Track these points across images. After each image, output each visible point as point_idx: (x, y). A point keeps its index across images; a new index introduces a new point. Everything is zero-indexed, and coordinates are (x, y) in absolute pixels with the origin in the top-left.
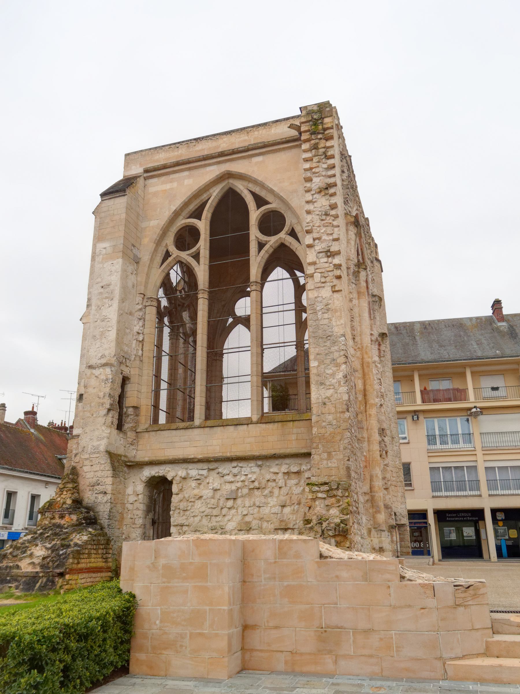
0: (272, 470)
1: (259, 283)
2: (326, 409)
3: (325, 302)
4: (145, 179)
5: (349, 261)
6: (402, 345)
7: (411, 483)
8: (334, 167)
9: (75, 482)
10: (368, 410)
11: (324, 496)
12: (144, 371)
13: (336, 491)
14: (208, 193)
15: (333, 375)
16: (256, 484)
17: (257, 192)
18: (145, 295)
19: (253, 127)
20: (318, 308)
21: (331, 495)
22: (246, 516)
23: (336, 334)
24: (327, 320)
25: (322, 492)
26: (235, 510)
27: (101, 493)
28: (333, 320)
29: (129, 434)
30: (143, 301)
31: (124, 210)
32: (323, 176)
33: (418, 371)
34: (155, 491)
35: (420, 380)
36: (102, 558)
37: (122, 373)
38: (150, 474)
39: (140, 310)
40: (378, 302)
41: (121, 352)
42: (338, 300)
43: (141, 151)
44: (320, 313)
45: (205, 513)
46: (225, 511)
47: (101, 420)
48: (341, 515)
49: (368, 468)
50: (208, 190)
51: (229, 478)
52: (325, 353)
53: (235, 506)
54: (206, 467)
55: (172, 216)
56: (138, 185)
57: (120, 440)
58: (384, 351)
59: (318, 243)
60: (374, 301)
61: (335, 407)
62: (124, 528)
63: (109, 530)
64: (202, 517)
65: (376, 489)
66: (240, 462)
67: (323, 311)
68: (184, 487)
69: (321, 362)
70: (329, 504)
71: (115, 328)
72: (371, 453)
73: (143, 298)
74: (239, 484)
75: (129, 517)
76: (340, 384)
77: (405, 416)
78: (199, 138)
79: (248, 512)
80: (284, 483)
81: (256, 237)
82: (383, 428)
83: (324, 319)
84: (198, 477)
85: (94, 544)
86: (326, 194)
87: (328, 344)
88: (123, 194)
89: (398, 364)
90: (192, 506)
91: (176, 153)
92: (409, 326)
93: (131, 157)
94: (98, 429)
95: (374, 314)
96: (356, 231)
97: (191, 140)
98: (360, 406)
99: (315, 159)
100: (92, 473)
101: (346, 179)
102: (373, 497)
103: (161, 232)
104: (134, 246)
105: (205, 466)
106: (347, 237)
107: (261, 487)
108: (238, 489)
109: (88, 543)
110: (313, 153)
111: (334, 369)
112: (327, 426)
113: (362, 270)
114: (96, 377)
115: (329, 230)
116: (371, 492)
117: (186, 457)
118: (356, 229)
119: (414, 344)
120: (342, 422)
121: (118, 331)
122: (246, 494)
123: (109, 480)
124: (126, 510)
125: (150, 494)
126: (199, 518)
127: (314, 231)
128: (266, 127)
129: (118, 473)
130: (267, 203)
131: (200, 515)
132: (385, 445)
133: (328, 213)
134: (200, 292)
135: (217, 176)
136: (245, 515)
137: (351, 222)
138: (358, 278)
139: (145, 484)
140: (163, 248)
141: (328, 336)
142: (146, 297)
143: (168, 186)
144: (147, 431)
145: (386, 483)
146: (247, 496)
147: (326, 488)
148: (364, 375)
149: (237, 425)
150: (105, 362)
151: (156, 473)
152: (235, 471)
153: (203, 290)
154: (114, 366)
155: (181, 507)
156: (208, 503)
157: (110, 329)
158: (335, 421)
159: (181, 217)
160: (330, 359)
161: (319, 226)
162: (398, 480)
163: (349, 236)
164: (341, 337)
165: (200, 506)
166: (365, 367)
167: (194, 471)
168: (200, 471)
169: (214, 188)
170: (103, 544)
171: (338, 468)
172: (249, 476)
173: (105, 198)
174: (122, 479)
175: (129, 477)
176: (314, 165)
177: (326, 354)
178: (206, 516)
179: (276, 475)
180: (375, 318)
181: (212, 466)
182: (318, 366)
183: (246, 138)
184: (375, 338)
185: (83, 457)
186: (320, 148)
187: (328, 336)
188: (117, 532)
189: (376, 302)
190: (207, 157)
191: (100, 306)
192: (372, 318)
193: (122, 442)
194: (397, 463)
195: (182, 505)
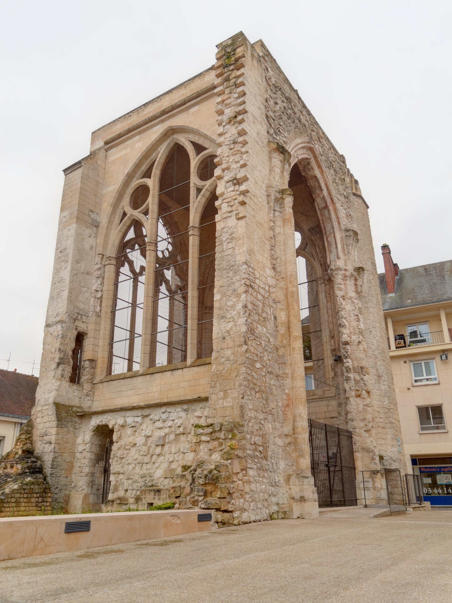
0: (196, 414)
1: (196, 227)
2: (225, 344)
3: (230, 231)
4: (107, 150)
5: (269, 188)
6: (430, 285)
7: (445, 426)
8: (245, 94)
9: (28, 433)
10: (291, 343)
11: (208, 439)
12: (101, 326)
13: (219, 433)
15: (233, 306)
16: (181, 429)
17: (196, 142)
18: (104, 255)
19: (190, 80)
20: (224, 239)
21: (214, 438)
22: (173, 463)
23: (238, 262)
24: (231, 250)
25: (206, 435)
26: (163, 457)
28: (236, 249)
30: (102, 261)
32: (234, 106)
33: (444, 309)
34: (108, 440)
35: (447, 318)
36: (36, 506)
37: (76, 329)
38: (96, 423)
39: (99, 269)
40: (352, 237)
41: (75, 309)
42: (241, 227)
43: (104, 127)
44: (226, 243)
45: (137, 461)
46: (155, 457)
47: (52, 374)
48: (222, 460)
49: (292, 407)
50: (156, 149)
51: (159, 424)
52: (227, 285)
53: (163, 453)
54: (140, 414)
56: (97, 156)
58: (361, 286)
59: (227, 173)
60: (347, 236)
61: (233, 341)
62: (74, 476)
63: (51, 479)
64: (135, 465)
65: (299, 430)
66: (168, 407)
67: (228, 241)
68: (122, 434)
69: (224, 295)
70: (212, 448)
72: (294, 390)
73: (102, 258)
74: (167, 430)
75: (78, 466)
76: (239, 315)
77: (432, 356)
79: (174, 458)
82: (361, 366)
83: (229, 249)
84: (133, 425)
85: (25, 493)
86: (235, 123)
87: (231, 274)
88: (79, 166)
89: (422, 304)
90: (127, 454)
91: (129, 121)
92: (439, 266)
93: (96, 134)
94: (49, 382)
95: (348, 248)
96: (281, 158)
97: (141, 106)
98: (282, 339)
99: (227, 91)
100: (42, 424)
101: (279, 110)
102: (296, 439)
103: (117, 195)
104: (92, 212)
105: (139, 413)
107: (186, 432)
108: (166, 436)
109: (16, 491)
110: (225, 86)
112: (225, 362)
113: (287, 196)
114: (51, 334)
115: (237, 158)
116: (294, 434)
117: (123, 406)
118: (282, 155)
119: (442, 283)
120: (239, 356)
122: (173, 440)
123: (54, 431)
124: (76, 459)
125: (100, 443)
126: (133, 465)
127: (224, 162)
129: (65, 423)
130: (205, 149)
131: (133, 462)
132: (364, 384)
133: (236, 141)
134: (147, 244)
137: (274, 149)
138: (282, 206)
139: (93, 434)
142: (105, 257)
143: (123, 153)
144: (101, 382)
145: (366, 425)
146: (174, 442)
147: (210, 430)
148: (288, 305)
149: (173, 370)
150: (59, 319)
151: (100, 422)
152: (164, 416)
153: (150, 242)
154: (65, 322)
155: (118, 455)
156: (140, 451)
157: (64, 289)
158: (233, 356)
159: (135, 179)
160: (231, 291)
161: (228, 156)
162: (387, 421)
163: (273, 164)
164: (243, 265)
166: (289, 297)
168: (136, 418)
169: (162, 146)
170: (38, 493)
171: (232, 407)
172: (176, 421)
174: (72, 429)
175: (81, 427)
176: (226, 96)
178: (139, 463)
179: (200, 418)
180: (349, 253)
182: (221, 299)
183: (184, 92)
184: (350, 273)
185: (37, 410)
186: (232, 79)
188: (63, 481)
189: (350, 236)
190: (152, 118)
192: (346, 253)
194: (385, 403)
195: (120, 453)
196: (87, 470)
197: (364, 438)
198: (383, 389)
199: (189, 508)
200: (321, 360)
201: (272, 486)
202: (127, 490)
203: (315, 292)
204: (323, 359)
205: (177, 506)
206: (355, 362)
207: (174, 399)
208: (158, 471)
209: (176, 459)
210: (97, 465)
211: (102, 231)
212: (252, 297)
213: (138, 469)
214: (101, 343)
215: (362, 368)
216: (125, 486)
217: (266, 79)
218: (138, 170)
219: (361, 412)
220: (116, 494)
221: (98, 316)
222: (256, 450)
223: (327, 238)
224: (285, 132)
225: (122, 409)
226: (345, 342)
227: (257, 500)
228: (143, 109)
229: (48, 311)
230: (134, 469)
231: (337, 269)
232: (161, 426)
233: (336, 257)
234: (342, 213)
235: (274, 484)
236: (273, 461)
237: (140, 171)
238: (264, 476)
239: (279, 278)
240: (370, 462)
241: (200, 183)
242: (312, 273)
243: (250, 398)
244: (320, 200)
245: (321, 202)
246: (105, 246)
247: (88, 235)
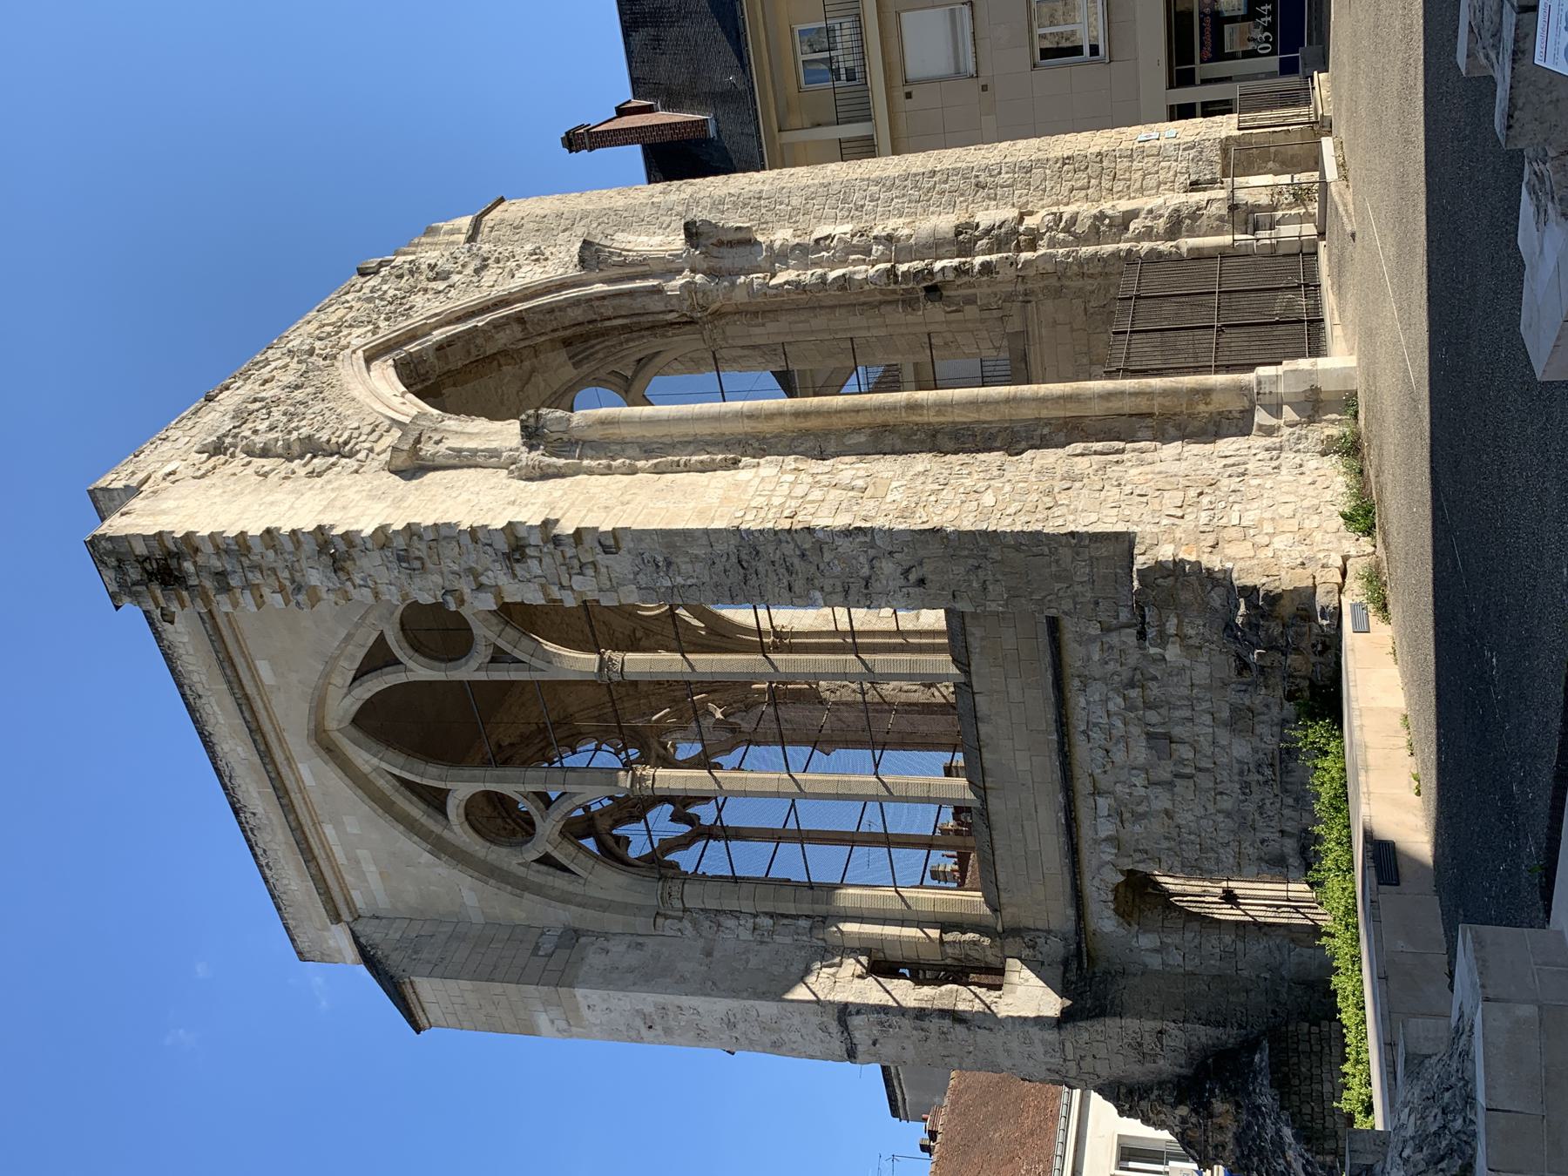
18: (658, 913)
31: (451, 983)
34: (1150, 890)
55: (445, 858)
63: (1252, 1027)
73: (666, 917)
74: (1135, 730)
78: (232, 805)
80: (1128, 630)
81: (477, 670)
93: (304, 944)
97: (240, 823)
103: (492, 882)
111: (827, 556)
123: (1132, 1024)
141: (742, 565)
143: (371, 869)
150: (835, 1023)
157: (755, 1013)
159: (446, 834)
167: (1097, 825)
172: (1111, 706)
177: (790, 571)
187: (742, 565)
191: (699, 1032)
200: (930, 340)
203: (746, 352)
204: (929, 334)
207: (1051, 715)
212: (820, 514)
217: (202, 476)
218: (422, 825)
224: (346, 428)
225: (1073, 851)
228: (248, 815)
229: (812, 1057)
234: (532, 274)
237: (424, 820)
241: (481, 653)
242: (692, 360)
244: (502, 334)
245: (508, 332)
247: (604, 955)
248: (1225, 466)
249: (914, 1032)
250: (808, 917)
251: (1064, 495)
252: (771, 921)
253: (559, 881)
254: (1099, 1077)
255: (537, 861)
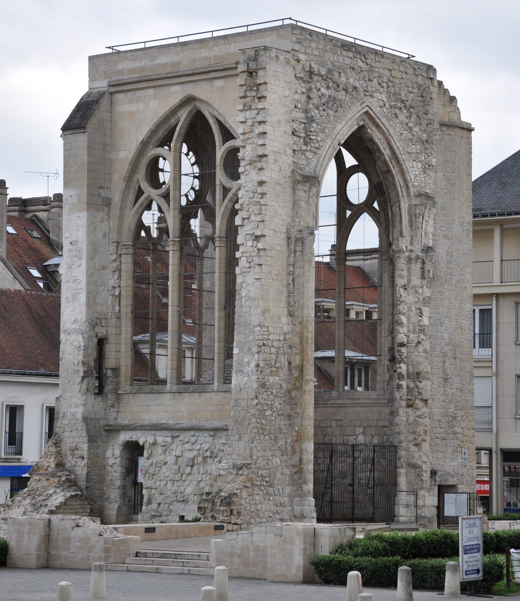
0: (221, 441)
12: (122, 329)
14: (176, 117)
15: (249, 363)
22: (201, 482)
26: (193, 476)
27: (80, 457)
29: (109, 396)
30: (117, 250)
34: (136, 453)
37: (97, 336)
38: (125, 438)
39: (115, 260)
45: (169, 478)
47: (77, 387)
51: (187, 446)
55: (140, 146)
57: (99, 404)
64: (167, 481)
69: (241, 350)
71: (85, 291)
73: (117, 247)
74: (195, 453)
84: (163, 444)
94: (75, 396)
100: (72, 439)
102: (302, 469)
103: (130, 167)
105: (169, 433)
106: (294, 198)
108: (194, 457)
116: (300, 464)
121: (88, 293)
123: (85, 446)
126: (165, 482)
128: (226, 42)
135: (181, 100)
136: (199, 481)
139: (122, 448)
140: (135, 183)
145: (415, 439)
151: (130, 438)
152: (193, 439)
157: (80, 292)
159: (151, 146)
163: (296, 197)
165: (165, 471)
167: (161, 438)
172: (204, 445)
173: (67, 133)
178: (170, 480)
181: (176, 434)
182: (239, 353)
193: (101, 406)
194: (449, 411)
196: (118, 483)
197: (411, 453)
198: (450, 393)
199: (211, 522)
201: (277, 506)
202: (160, 504)
205: (202, 520)
206: (410, 367)
208: (188, 488)
209: (204, 479)
210: (127, 478)
211: (115, 211)
213: (169, 484)
214: (123, 349)
215: (418, 374)
216: (158, 500)
219: (411, 424)
220: (149, 506)
221: (119, 318)
222: (263, 480)
223: (391, 207)
226: (400, 343)
227: (262, 517)
230: (166, 485)
231: (399, 251)
232: (190, 448)
233: (399, 234)
235: (278, 505)
236: (279, 487)
238: (269, 500)
239: (296, 322)
240: (415, 478)
243: (259, 441)
244: (381, 163)
246: (120, 232)
248: (279, 489)
249: (77, 360)
250: (120, 310)
251: (268, 438)
252: (117, 294)
253: (131, 197)
254: (63, 432)
255: (140, 187)
